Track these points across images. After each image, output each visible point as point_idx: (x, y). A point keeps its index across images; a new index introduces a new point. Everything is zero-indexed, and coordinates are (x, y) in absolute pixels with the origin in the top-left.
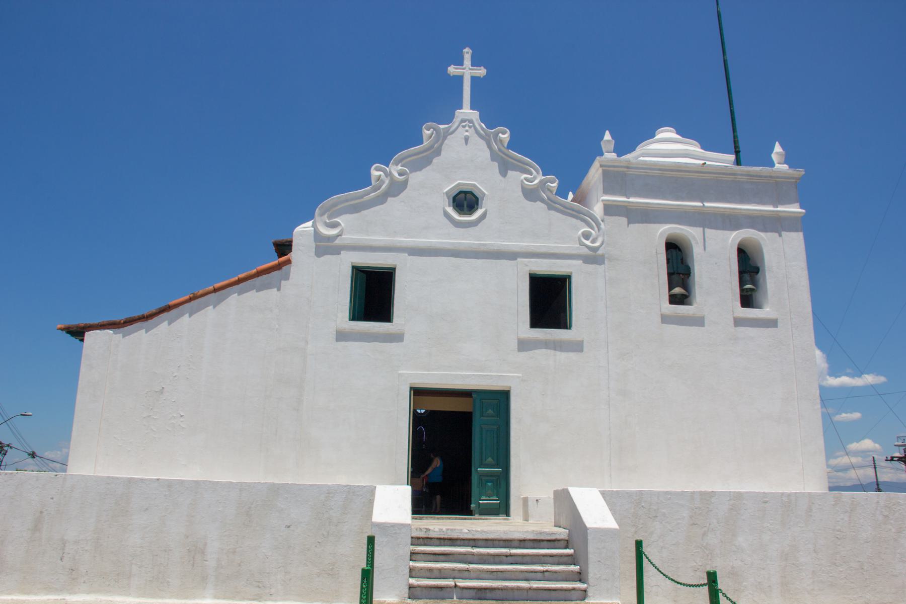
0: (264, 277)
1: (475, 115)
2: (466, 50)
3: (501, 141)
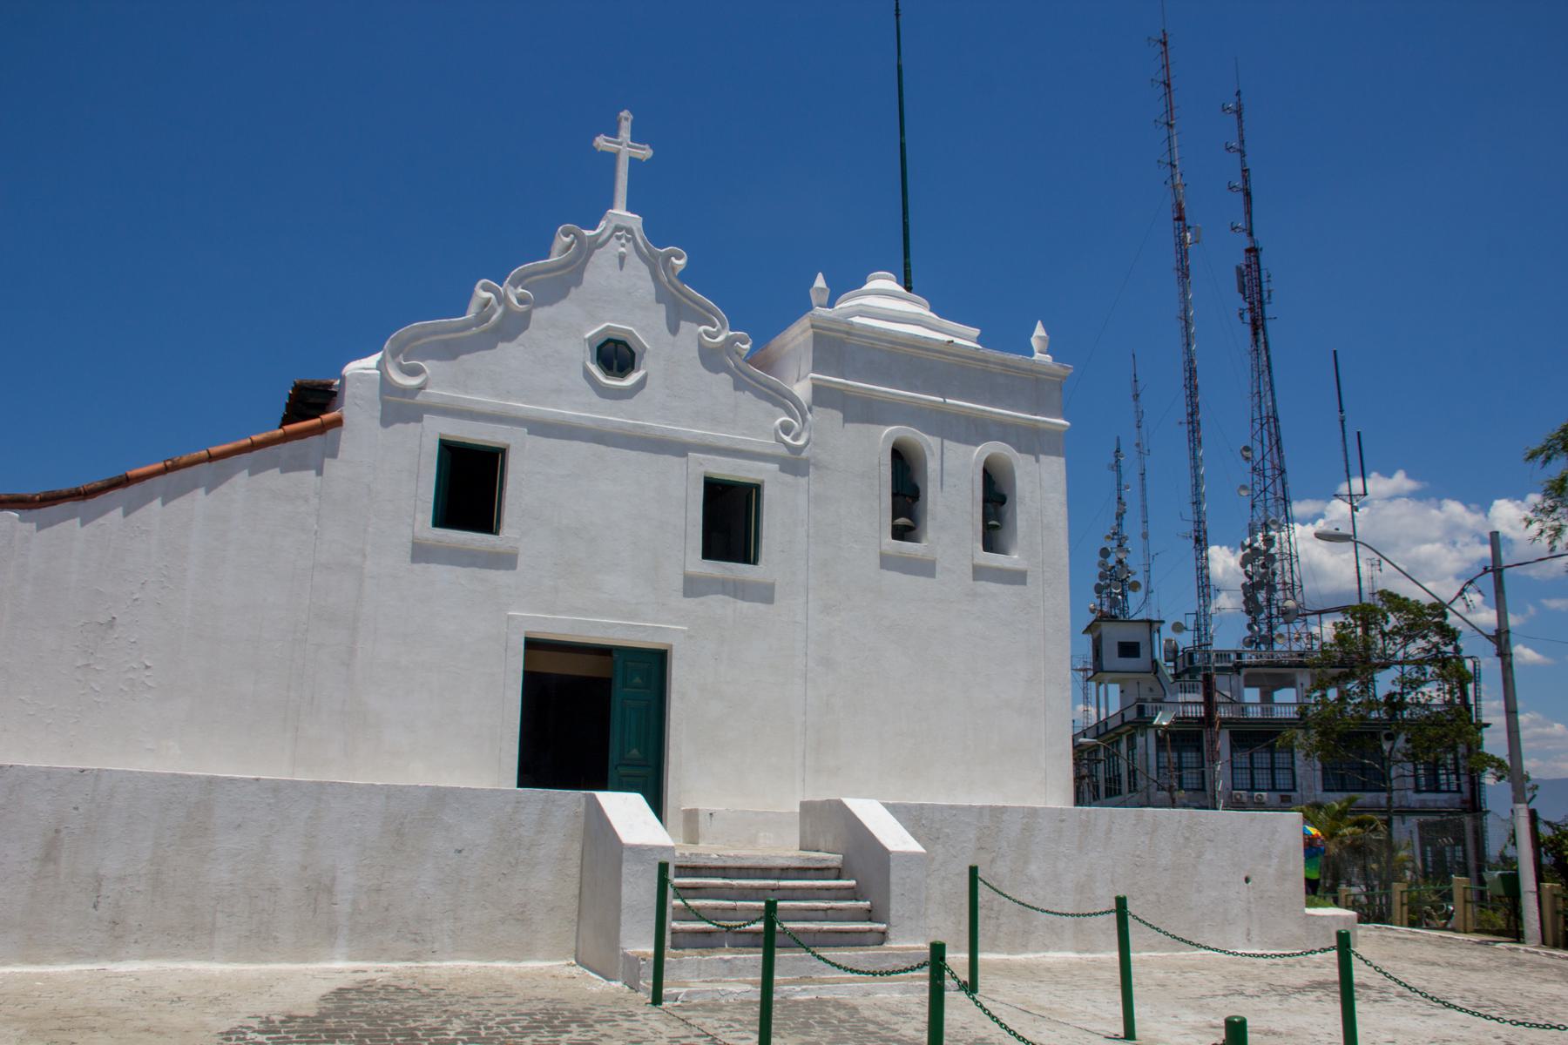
0: (296, 443)
1: (635, 221)
2: (625, 114)
3: (673, 268)
